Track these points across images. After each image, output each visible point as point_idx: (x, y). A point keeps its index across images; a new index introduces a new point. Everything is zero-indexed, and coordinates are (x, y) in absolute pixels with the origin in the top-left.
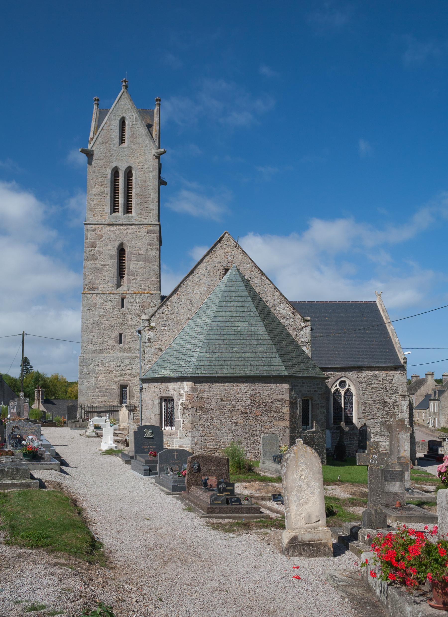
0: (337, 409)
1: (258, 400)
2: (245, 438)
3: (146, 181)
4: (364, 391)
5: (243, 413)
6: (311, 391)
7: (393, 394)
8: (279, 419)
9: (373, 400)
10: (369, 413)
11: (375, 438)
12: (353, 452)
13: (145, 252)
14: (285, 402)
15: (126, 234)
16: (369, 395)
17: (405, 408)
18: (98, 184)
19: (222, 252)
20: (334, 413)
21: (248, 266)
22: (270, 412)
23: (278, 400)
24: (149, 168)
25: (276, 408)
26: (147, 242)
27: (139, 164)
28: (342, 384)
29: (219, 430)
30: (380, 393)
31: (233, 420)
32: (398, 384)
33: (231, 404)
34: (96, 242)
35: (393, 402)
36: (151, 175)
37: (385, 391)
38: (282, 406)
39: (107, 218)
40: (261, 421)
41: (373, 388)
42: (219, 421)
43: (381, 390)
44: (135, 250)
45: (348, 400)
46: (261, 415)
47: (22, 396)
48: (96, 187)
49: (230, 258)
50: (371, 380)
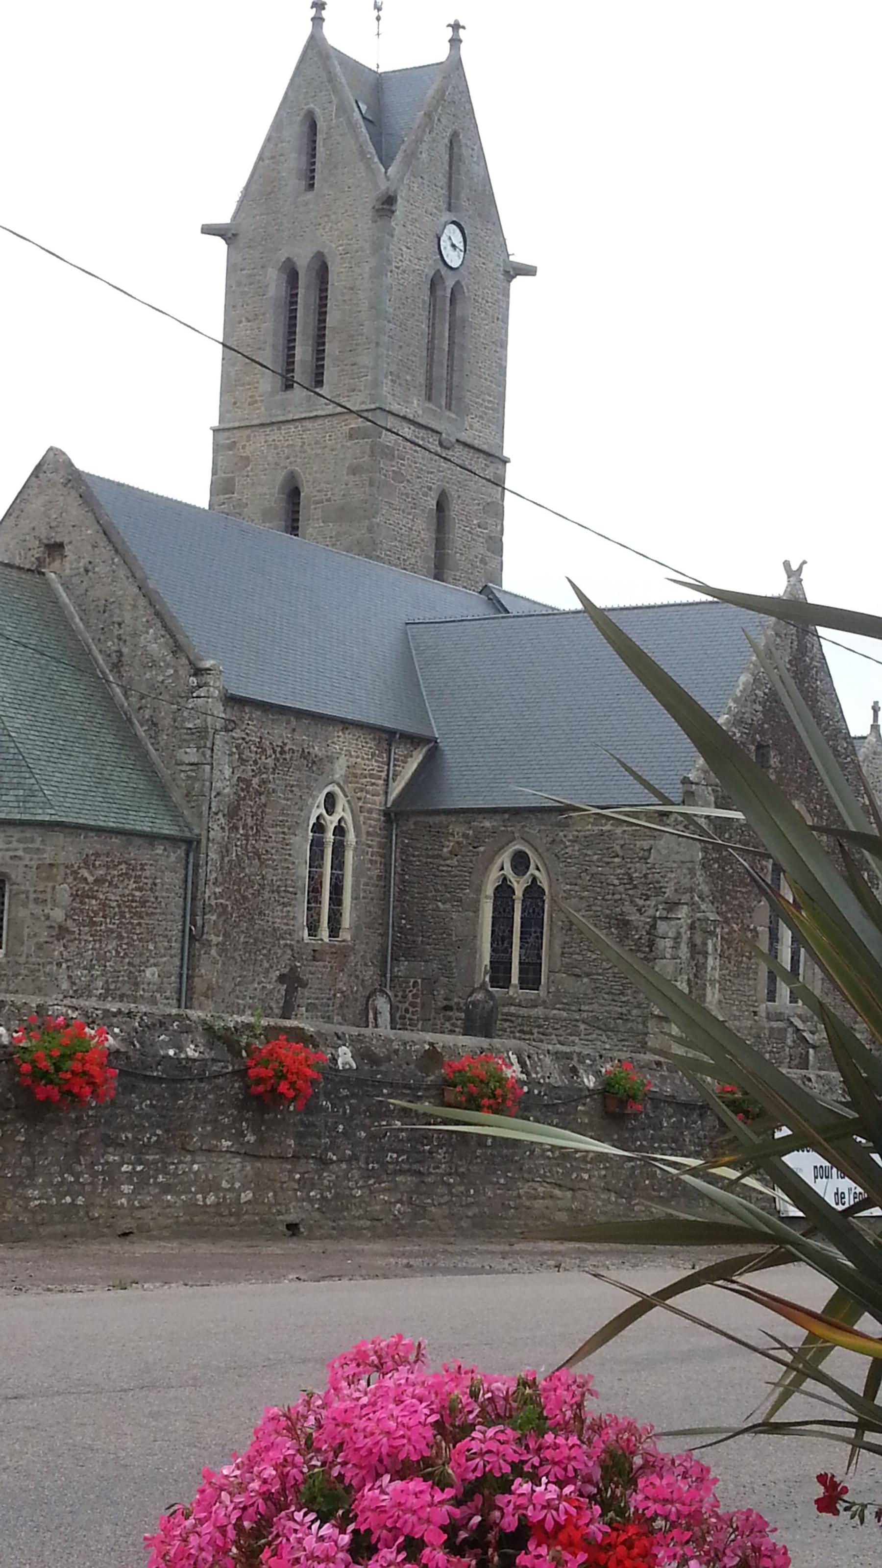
0: (503, 939)
3: (352, 289)
10: (580, 958)
11: (589, 1037)
13: (342, 493)
15: (302, 446)
18: (247, 315)
20: (493, 950)
21: (89, 532)
27: (341, 242)
30: (613, 894)
32: (668, 865)
34: (233, 479)
35: (648, 923)
36: (367, 269)
37: (628, 886)
39: (263, 409)
43: (616, 882)
44: (319, 491)
45: (534, 912)
48: (241, 325)
49: (54, 516)
50: (589, 852)
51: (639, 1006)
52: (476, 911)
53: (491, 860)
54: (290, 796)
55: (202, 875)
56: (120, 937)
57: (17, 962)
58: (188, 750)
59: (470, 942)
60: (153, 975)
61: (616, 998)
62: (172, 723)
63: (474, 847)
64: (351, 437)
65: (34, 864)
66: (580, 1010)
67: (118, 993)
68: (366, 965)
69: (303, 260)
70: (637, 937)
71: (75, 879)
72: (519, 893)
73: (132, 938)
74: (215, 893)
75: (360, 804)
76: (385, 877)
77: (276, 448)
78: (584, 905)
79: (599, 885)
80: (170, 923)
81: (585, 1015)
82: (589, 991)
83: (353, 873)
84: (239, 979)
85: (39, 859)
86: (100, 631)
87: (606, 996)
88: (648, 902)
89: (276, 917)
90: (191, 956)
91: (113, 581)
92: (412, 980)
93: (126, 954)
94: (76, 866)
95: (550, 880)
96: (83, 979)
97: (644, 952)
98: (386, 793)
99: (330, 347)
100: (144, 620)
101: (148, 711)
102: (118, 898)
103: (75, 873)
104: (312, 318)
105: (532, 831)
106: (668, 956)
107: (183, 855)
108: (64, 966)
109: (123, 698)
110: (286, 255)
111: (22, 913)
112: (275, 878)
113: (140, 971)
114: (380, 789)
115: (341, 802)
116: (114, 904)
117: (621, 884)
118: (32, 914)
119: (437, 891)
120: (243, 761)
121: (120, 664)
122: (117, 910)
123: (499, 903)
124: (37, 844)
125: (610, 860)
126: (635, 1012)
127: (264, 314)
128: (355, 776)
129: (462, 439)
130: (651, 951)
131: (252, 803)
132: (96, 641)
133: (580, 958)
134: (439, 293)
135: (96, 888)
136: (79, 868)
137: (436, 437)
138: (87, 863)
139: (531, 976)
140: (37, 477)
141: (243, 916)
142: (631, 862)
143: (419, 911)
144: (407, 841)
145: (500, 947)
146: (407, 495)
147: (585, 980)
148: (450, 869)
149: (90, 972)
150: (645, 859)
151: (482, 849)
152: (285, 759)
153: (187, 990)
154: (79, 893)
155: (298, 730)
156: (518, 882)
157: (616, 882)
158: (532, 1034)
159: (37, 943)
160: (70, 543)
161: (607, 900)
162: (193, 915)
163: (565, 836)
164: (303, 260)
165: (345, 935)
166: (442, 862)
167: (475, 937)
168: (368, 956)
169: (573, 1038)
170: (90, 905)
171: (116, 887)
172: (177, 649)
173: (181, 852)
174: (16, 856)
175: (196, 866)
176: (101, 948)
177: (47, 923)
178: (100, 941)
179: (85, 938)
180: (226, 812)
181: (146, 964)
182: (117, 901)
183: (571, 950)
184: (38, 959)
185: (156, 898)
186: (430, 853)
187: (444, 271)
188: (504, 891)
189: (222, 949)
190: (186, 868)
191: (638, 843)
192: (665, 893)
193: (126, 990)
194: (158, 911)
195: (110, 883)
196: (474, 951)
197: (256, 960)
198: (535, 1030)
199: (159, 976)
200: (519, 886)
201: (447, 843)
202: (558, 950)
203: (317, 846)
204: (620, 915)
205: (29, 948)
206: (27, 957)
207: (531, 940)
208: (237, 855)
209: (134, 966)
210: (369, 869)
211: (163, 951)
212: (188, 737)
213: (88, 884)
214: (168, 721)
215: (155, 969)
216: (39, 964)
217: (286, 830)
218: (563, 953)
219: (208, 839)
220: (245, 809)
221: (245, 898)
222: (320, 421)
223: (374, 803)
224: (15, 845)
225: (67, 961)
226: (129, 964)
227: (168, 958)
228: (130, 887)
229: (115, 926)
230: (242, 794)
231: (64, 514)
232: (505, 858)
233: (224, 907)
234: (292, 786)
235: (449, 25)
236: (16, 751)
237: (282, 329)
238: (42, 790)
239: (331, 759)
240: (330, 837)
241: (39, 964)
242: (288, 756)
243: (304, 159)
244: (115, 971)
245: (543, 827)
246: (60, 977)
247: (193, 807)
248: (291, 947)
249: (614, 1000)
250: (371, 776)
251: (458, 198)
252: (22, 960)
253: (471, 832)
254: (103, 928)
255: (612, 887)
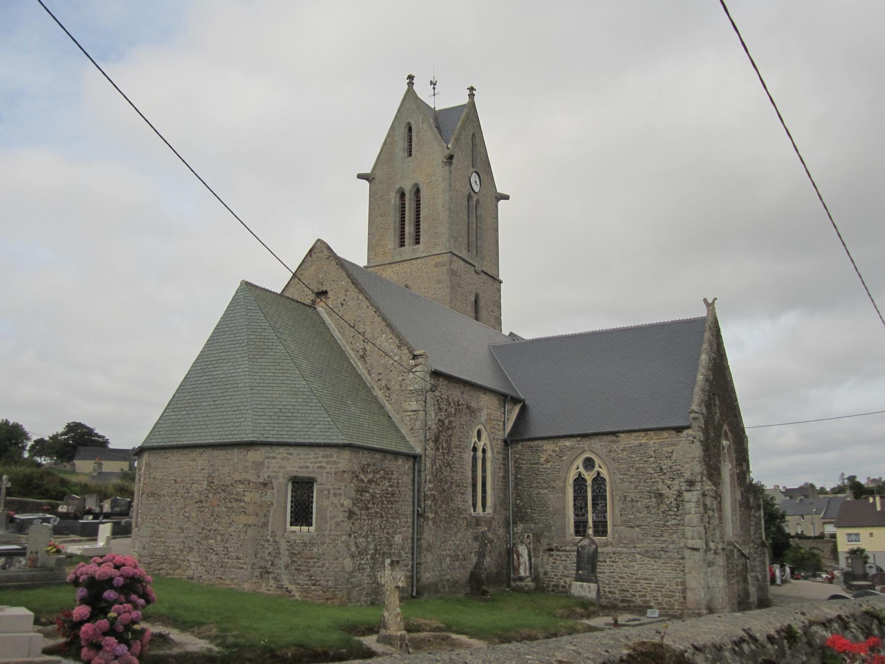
0: (581, 508)
1: (216, 482)
2: (197, 542)
3: (433, 198)
4: (623, 475)
5: (197, 502)
6: (308, 467)
7: (673, 479)
8: (240, 512)
9: (638, 492)
10: (633, 517)
11: (643, 563)
12: (605, 587)
14: (249, 483)
16: (631, 482)
17: (692, 506)
19: (313, 268)
21: (343, 283)
22: (230, 500)
23: (240, 481)
24: (437, 180)
25: (237, 494)
26: (435, 279)
28: (589, 464)
29: (169, 528)
30: (651, 479)
31: (185, 512)
32: (685, 460)
33: (185, 488)
35: (675, 494)
36: (440, 189)
37: (660, 474)
38: (245, 491)
40: (217, 515)
41: (637, 469)
42: (170, 514)
43: (653, 472)
46: (218, 506)
47: (5, 480)
49: (321, 276)
50: (633, 456)
51: (673, 543)
52: (564, 493)
53: (572, 463)
54: (462, 430)
55: (423, 478)
56: (382, 516)
57: (323, 535)
58: (411, 403)
59: (560, 512)
60: (399, 539)
61: (658, 539)
62: (399, 387)
63: (560, 457)
64: (436, 266)
65: (333, 471)
66: (635, 547)
67: (382, 551)
68: (500, 527)
69: (408, 187)
70: (668, 502)
71: (357, 481)
72: (589, 482)
73: (388, 517)
74: (429, 488)
75: (493, 436)
76: (506, 477)
77: (398, 273)
78: (633, 486)
79: (642, 474)
80: (406, 507)
81: (639, 550)
82: (640, 536)
83: (491, 474)
84: (443, 539)
85: (337, 468)
86: (352, 338)
87: (651, 538)
88: (674, 482)
89: (458, 502)
90: (419, 526)
91: (358, 309)
92: (526, 535)
93: (385, 527)
94: (358, 472)
95: (609, 474)
96: (363, 544)
97: (674, 511)
98: (504, 429)
99: (423, 226)
100: (379, 329)
101: (383, 381)
102: (380, 492)
103: (357, 476)
104: (413, 214)
105: (596, 446)
106: (692, 512)
107: (412, 465)
108: (353, 536)
109: (367, 375)
110: (399, 186)
111: (326, 503)
112: (457, 478)
113: (392, 537)
114: (501, 427)
115: (484, 435)
116: (378, 496)
117: (655, 472)
118: (332, 503)
119: (538, 483)
120: (440, 409)
121: (365, 356)
122: (379, 499)
123: (577, 488)
124: (335, 459)
125: (647, 459)
126: (671, 546)
127: (389, 213)
128: (490, 419)
129: (484, 270)
130: (678, 510)
131: (445, 434)
132: (349, 343)
133: (633, 517)
134: (471, 203)
135: (368, 486)
136: (359, 473)
137: (473, 268)
138: (363, 470)
139: (601, 529)
140: (311, 256)
141: (443, 501)
142: (661, 460)
143: (528, 495)
144: (517, 456)
145: (580, 513)
146: (462, 294)
147: (637, 529)
148: (545, 470)
149: (366, 539)
150: (670, 457)
151: (565, 458)
152: (459, 409)
153: (417, 547)
154: (360, 489)
155: (465, 393)
156: (589, 475)
157: (653, 472)
158: (606, 562)
159: (336, 522)
160: (332, 290)
161: (647, 483)
162: (419, 501)
163: (617, 447)
164: (408, 187)
165: (489, 510)
166: (541, 467)
167: (564, 508)
168: (501, 522)
169: (633, 563)
170: (366, 497)
171: (379, 485)
172: (402, 342)
173: (411, 463)
174: (321, 467)
175: (420, 471)
176: (372, 524)
177: (342, 509)
178: (371, 519)
179: (364, 517)
180: (433, 439)
181: (395, 532)
182: (379, 494)
183: (626, 513)
184: (337, 533)
185: (399, 492)
186: (533, 462)
187: (472, 193)
188: (579, 482)
189: (435, 522)
190: (414, 473)
191: (664, 449)
192: (684, 476)
193: (385, 550)
194: (401, 499)
195: (376, 483)
196: (564, 516)
197: (450, 527)
198: (608, 560)
199: (402, 540)
200: (589, 477)
201: (543, 456)
202: (618, 513)
203: (475, 459)
204: (657, 490)
205: (331, 526)
206: (330, 531)
207: (599, 508)
208: (439, 465)
209: (389, 534)
210: (498, 473)
211: (403, 524)
212: (410, 395)
213: (364, 483)
214: (397, 387)
215: (400, 535)
216: (338, 536)
217: (461, 450)
218: (621, 515)
219: (425, 455)
220: (442, 439)
221: (444, 490)
222: (419, 260)
223: (499, 435)
224: (320, 459)
225: (354, 533)
226: (388, 533)
227: (406, 528)
228: (386, 485)
229: (379, 510)
230: (441, 429)
231: (327, 275)
232: (579, 462)
233: (434, 496)
234: (463, 425)
235: (468, 89)
236: (317, 401)
237: (398, 220)
238: (336, 425)
239: (480, 410)
240: (480, 454)
241: (338, 536)
242: (461, 407)
243: (406, 143)
244: (380, 538)
245: (603, 443)
246: (350, 543)
247: (416, 436)
248: (466, 518)
249: (656, 540)
250: (498, 420)
251: (476, 162)
252: (327, 533)
253: (557, 449)
254: (373, 511)
255: (650, 475)
